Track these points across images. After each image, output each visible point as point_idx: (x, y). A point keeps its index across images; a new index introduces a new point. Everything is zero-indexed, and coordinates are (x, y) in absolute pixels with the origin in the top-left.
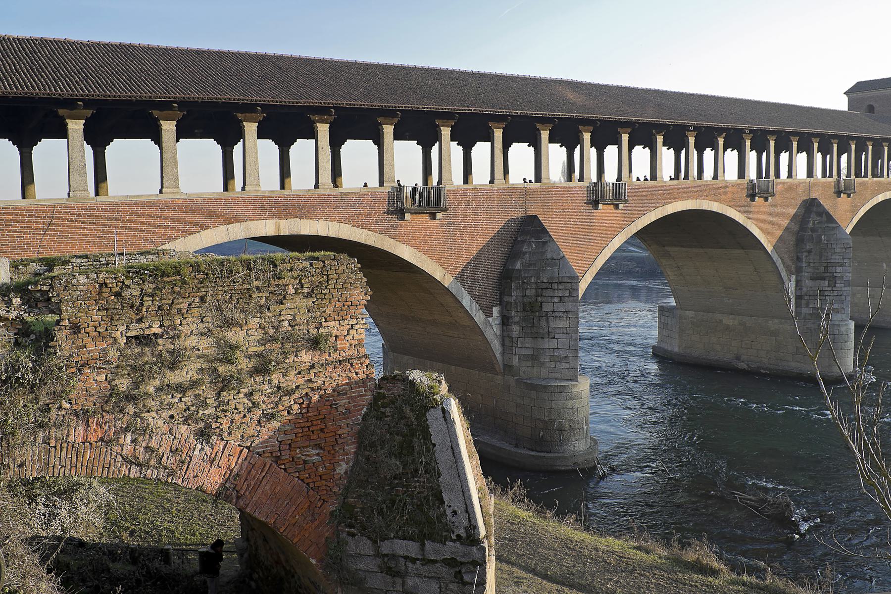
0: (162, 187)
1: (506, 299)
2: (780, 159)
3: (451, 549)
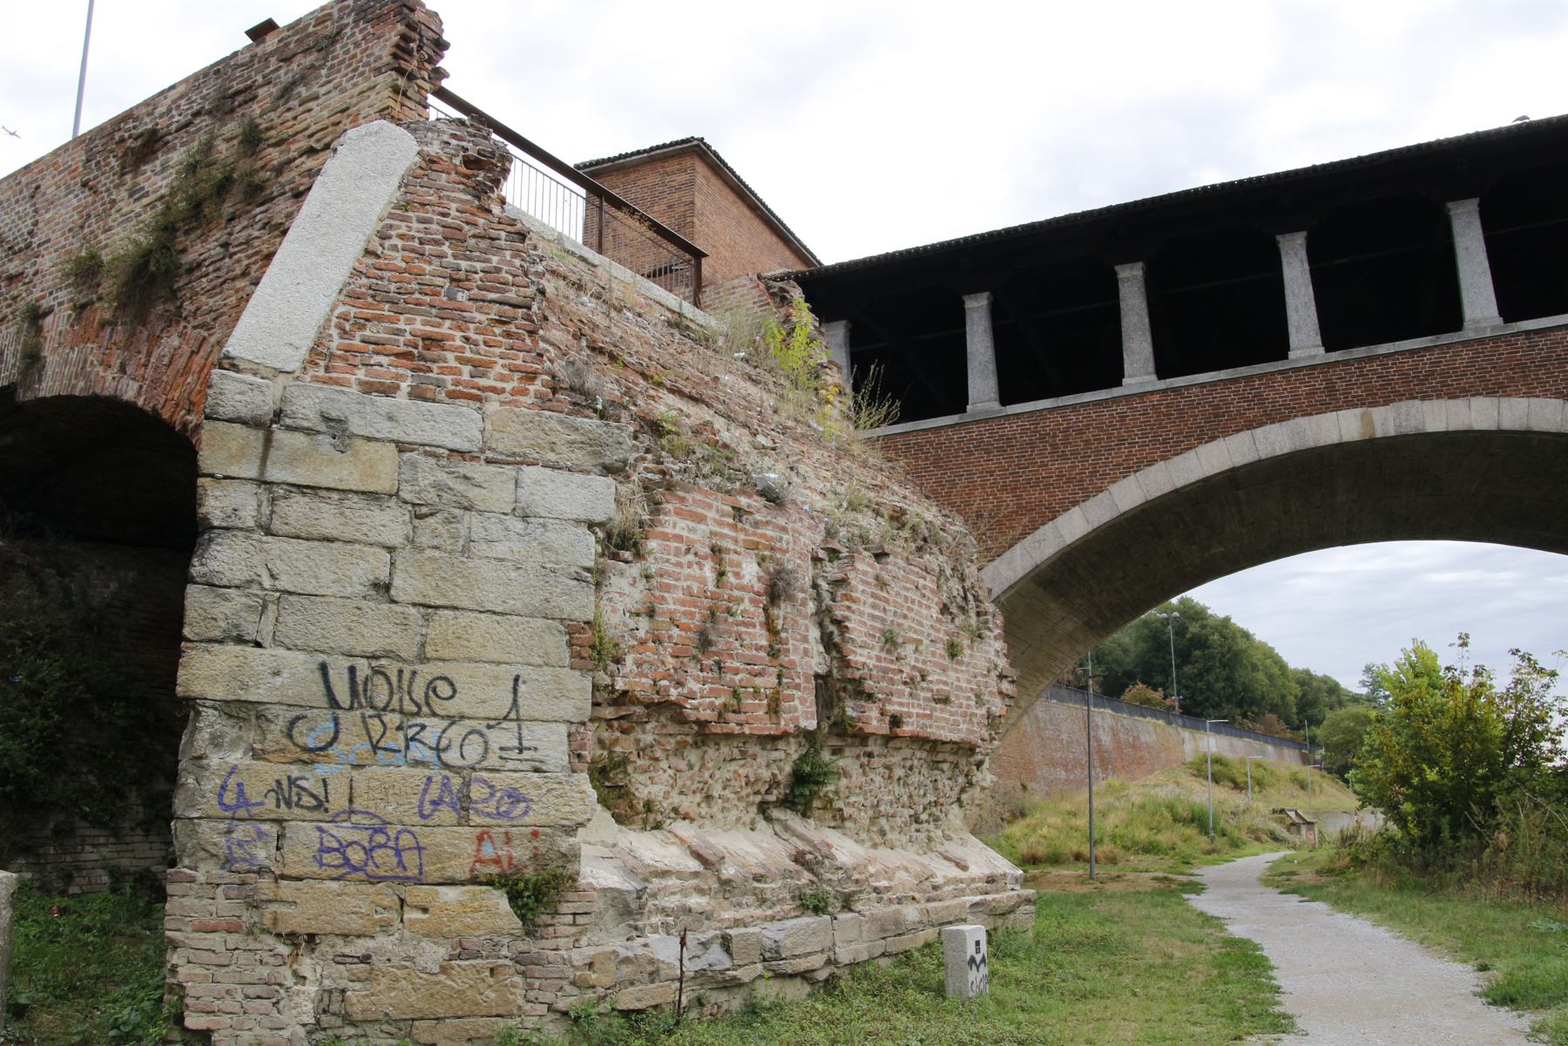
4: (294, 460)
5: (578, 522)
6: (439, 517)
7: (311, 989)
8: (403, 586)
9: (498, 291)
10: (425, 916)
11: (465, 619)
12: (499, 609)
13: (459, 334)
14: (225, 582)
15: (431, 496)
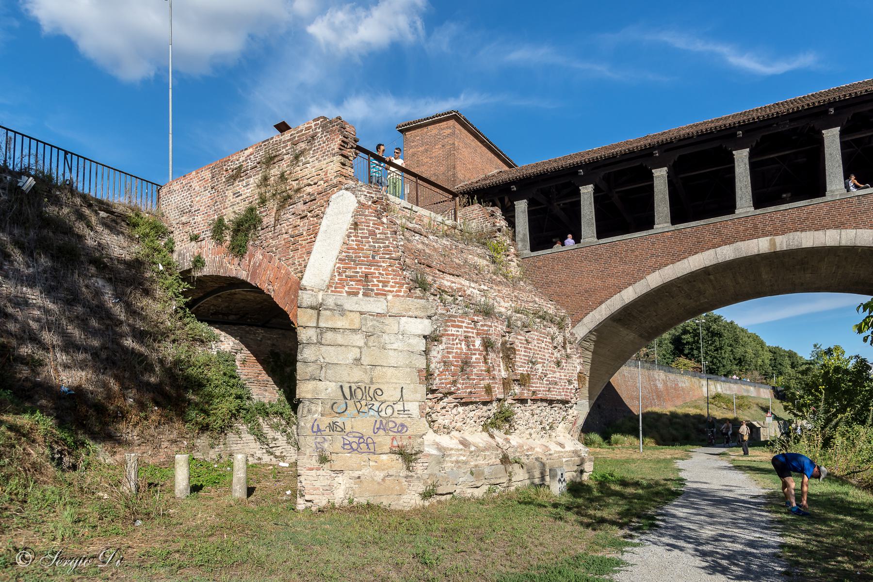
4: (327, 320)
5: (419, 336)
6: (375, 336)
7: (343, 487)
8: (365, 360)
9: (388, 254)
10: (377, 464)
11: (384, 370)
12: (395, 366)
13: (377, 272)
14: (309, 361)
15: (371, 330)
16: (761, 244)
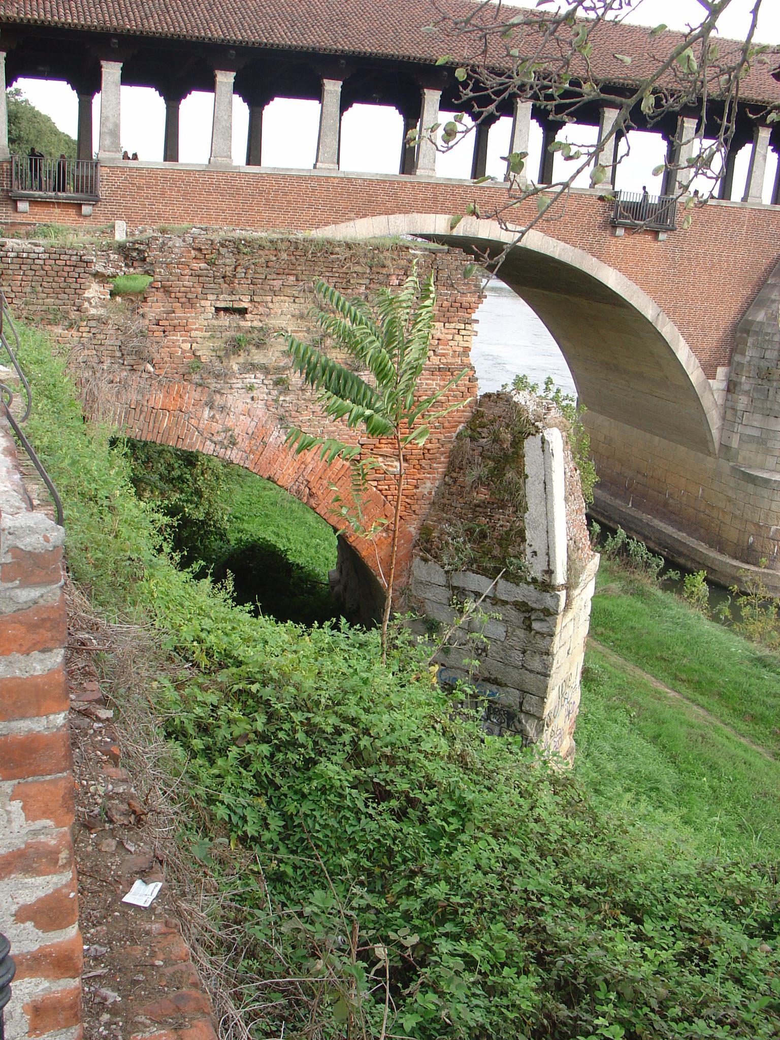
0: (317, 161)
1: (737, 358)
2: (149, 89)
3: (524, 593)
16: (438, 222)
